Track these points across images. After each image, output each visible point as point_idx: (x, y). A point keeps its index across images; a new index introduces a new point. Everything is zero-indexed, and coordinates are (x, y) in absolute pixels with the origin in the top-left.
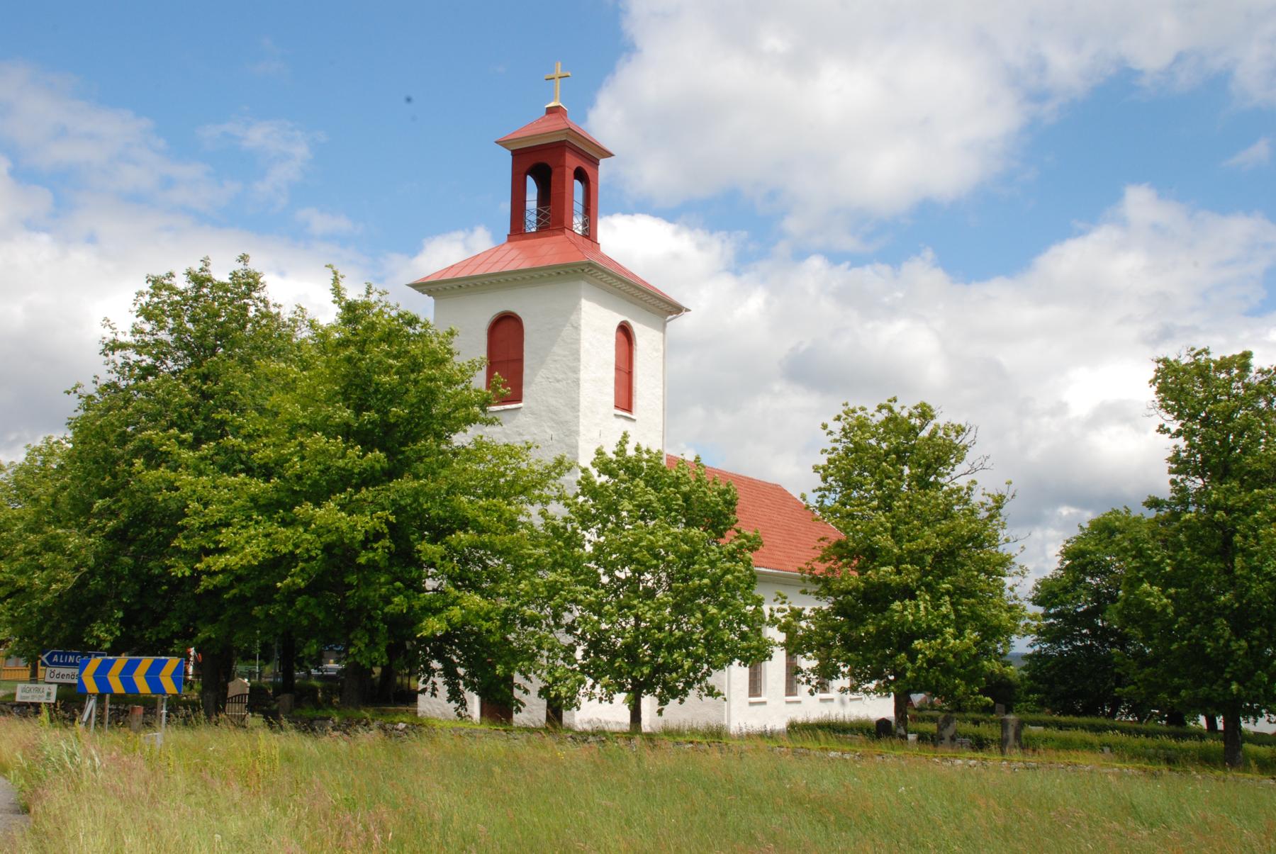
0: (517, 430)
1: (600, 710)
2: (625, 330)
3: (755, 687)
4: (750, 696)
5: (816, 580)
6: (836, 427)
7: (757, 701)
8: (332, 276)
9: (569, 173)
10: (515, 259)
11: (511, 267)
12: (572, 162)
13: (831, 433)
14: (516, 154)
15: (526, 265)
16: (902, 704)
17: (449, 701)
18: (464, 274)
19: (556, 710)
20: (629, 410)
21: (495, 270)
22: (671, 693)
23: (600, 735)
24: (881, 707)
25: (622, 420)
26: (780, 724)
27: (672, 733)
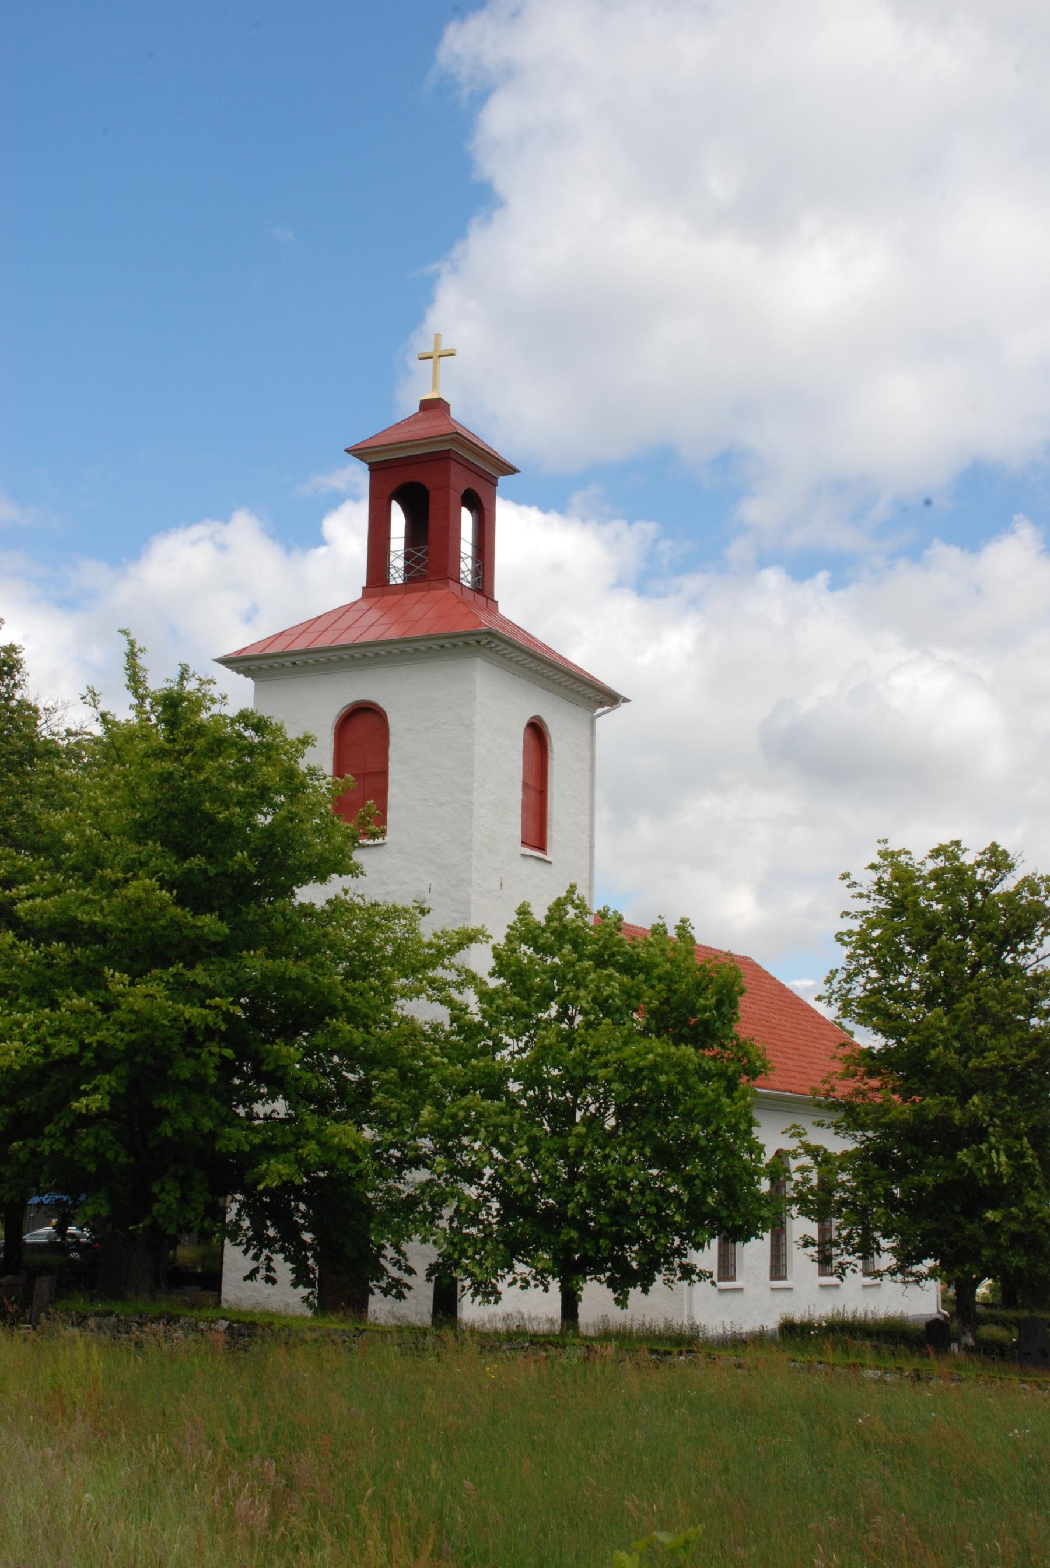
0: (382, 876)
1: (528, 1301)
2: (537, 731)
3: (778, 1268)
4: (772, 1278)
5: (835, 1106)
6: (868, 880)
7: (747, 1292)
8: (127, 648)
9: (456, 496)
10: (377, 627)
11: (370, 637)
12: (459, 482)
13: (854, 884)
14: (377, 470)
15: (392, 634)
16: (961, 1302)
17: (295, 1284)
18: (300, 645)
19: (445, 1303)
20: (541, 846)
21: (347, 639)
22: (623, 1281)
23: (517, 1339)
24: (921, 1300)
25: (533, 862)
26: (772, 1323)
27: (624, 1339)
